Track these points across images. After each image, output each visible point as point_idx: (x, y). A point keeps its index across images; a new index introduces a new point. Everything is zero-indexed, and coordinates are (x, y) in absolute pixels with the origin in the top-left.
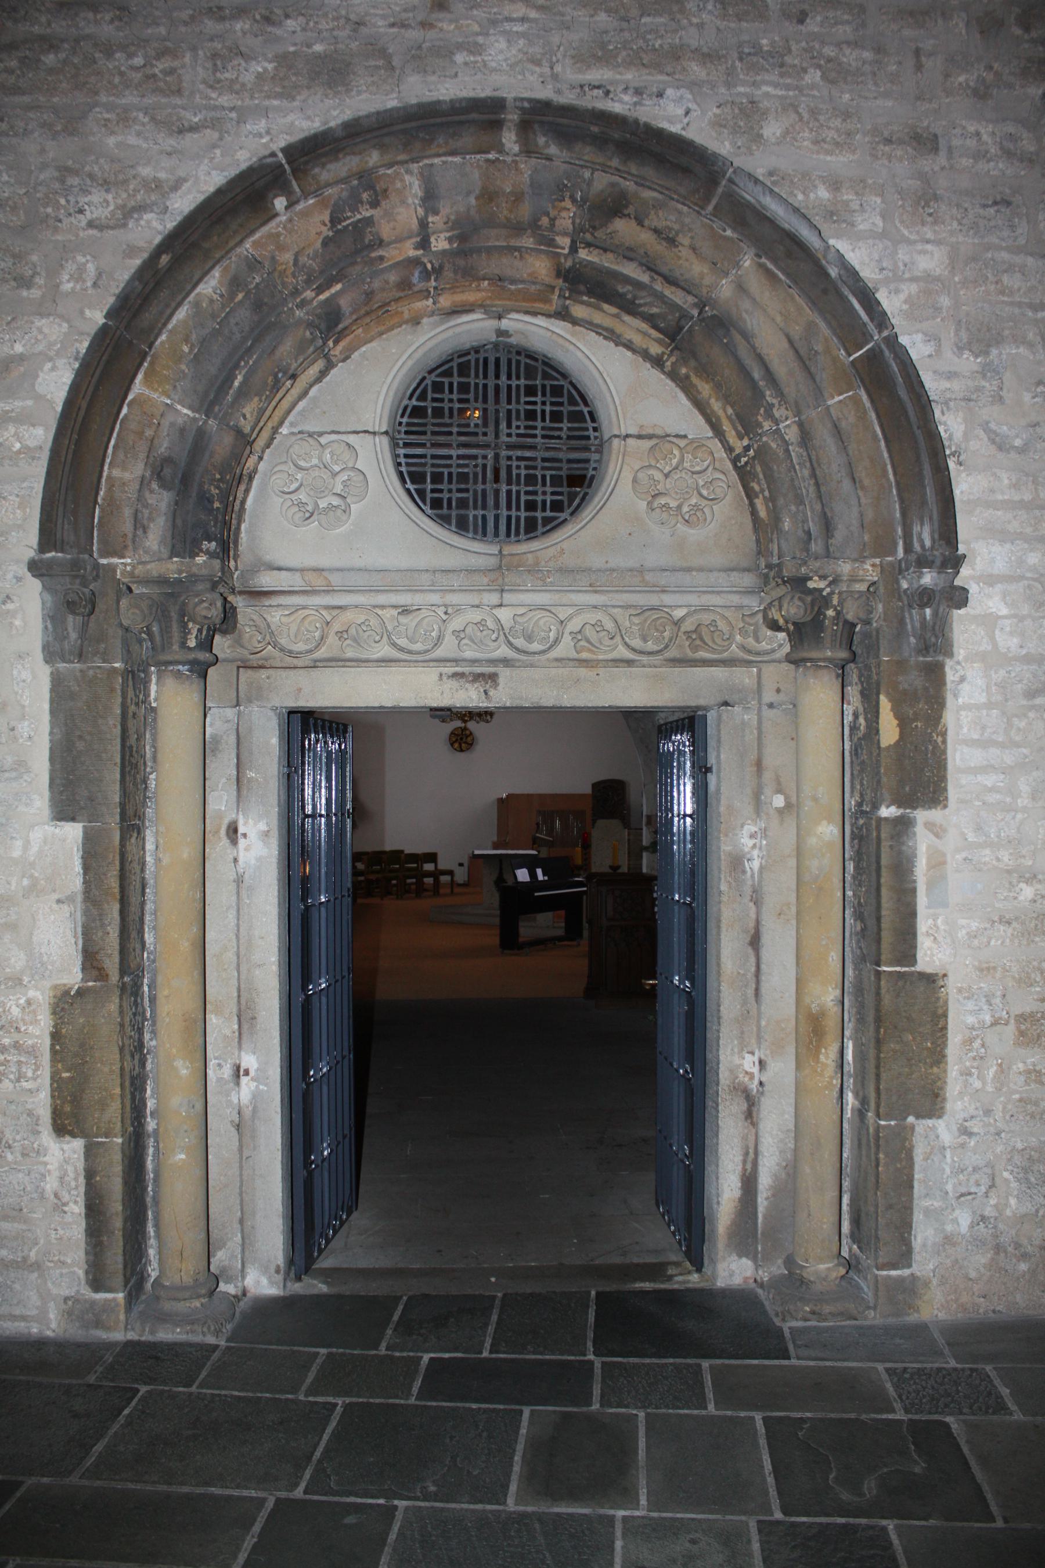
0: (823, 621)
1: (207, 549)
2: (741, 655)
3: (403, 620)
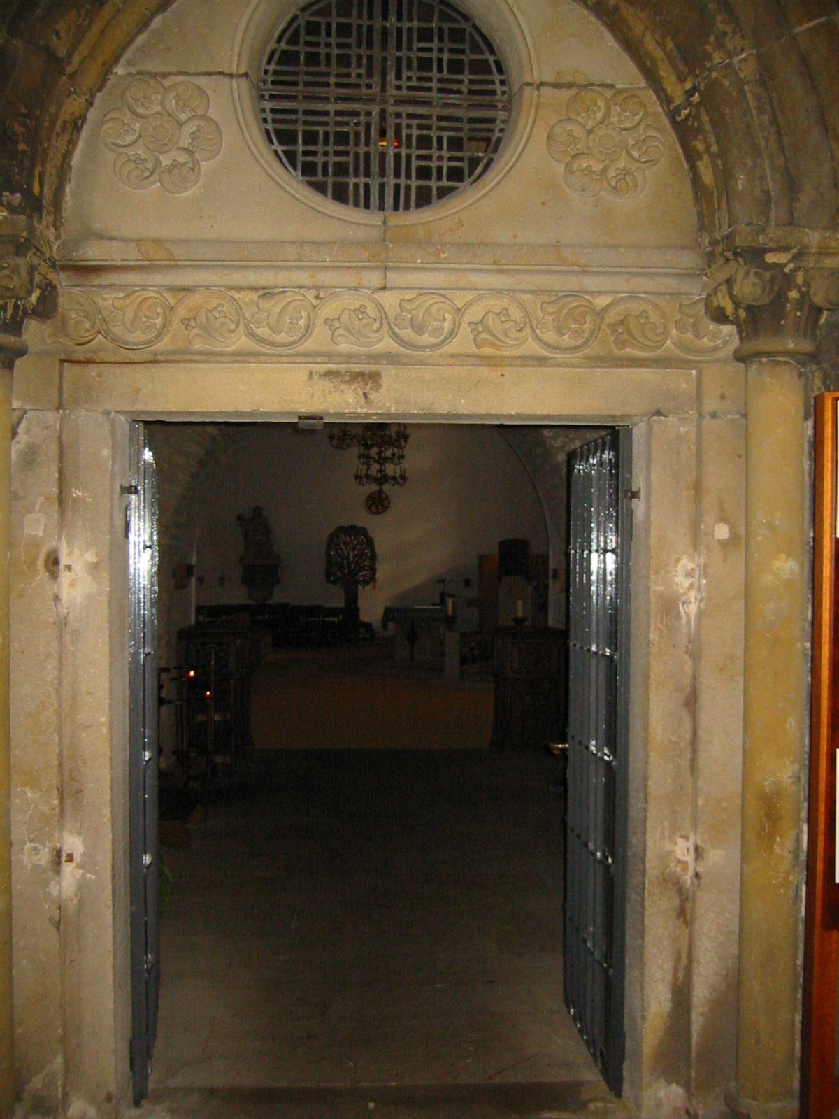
0: (784, 306)
1: (9, 203)
2: (677, 352)
3: (265, 304)
